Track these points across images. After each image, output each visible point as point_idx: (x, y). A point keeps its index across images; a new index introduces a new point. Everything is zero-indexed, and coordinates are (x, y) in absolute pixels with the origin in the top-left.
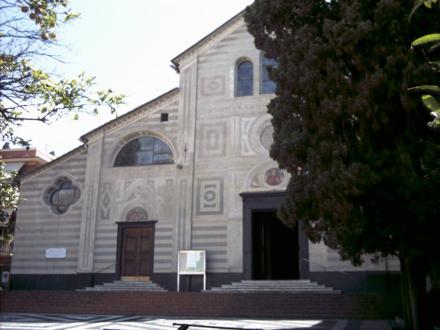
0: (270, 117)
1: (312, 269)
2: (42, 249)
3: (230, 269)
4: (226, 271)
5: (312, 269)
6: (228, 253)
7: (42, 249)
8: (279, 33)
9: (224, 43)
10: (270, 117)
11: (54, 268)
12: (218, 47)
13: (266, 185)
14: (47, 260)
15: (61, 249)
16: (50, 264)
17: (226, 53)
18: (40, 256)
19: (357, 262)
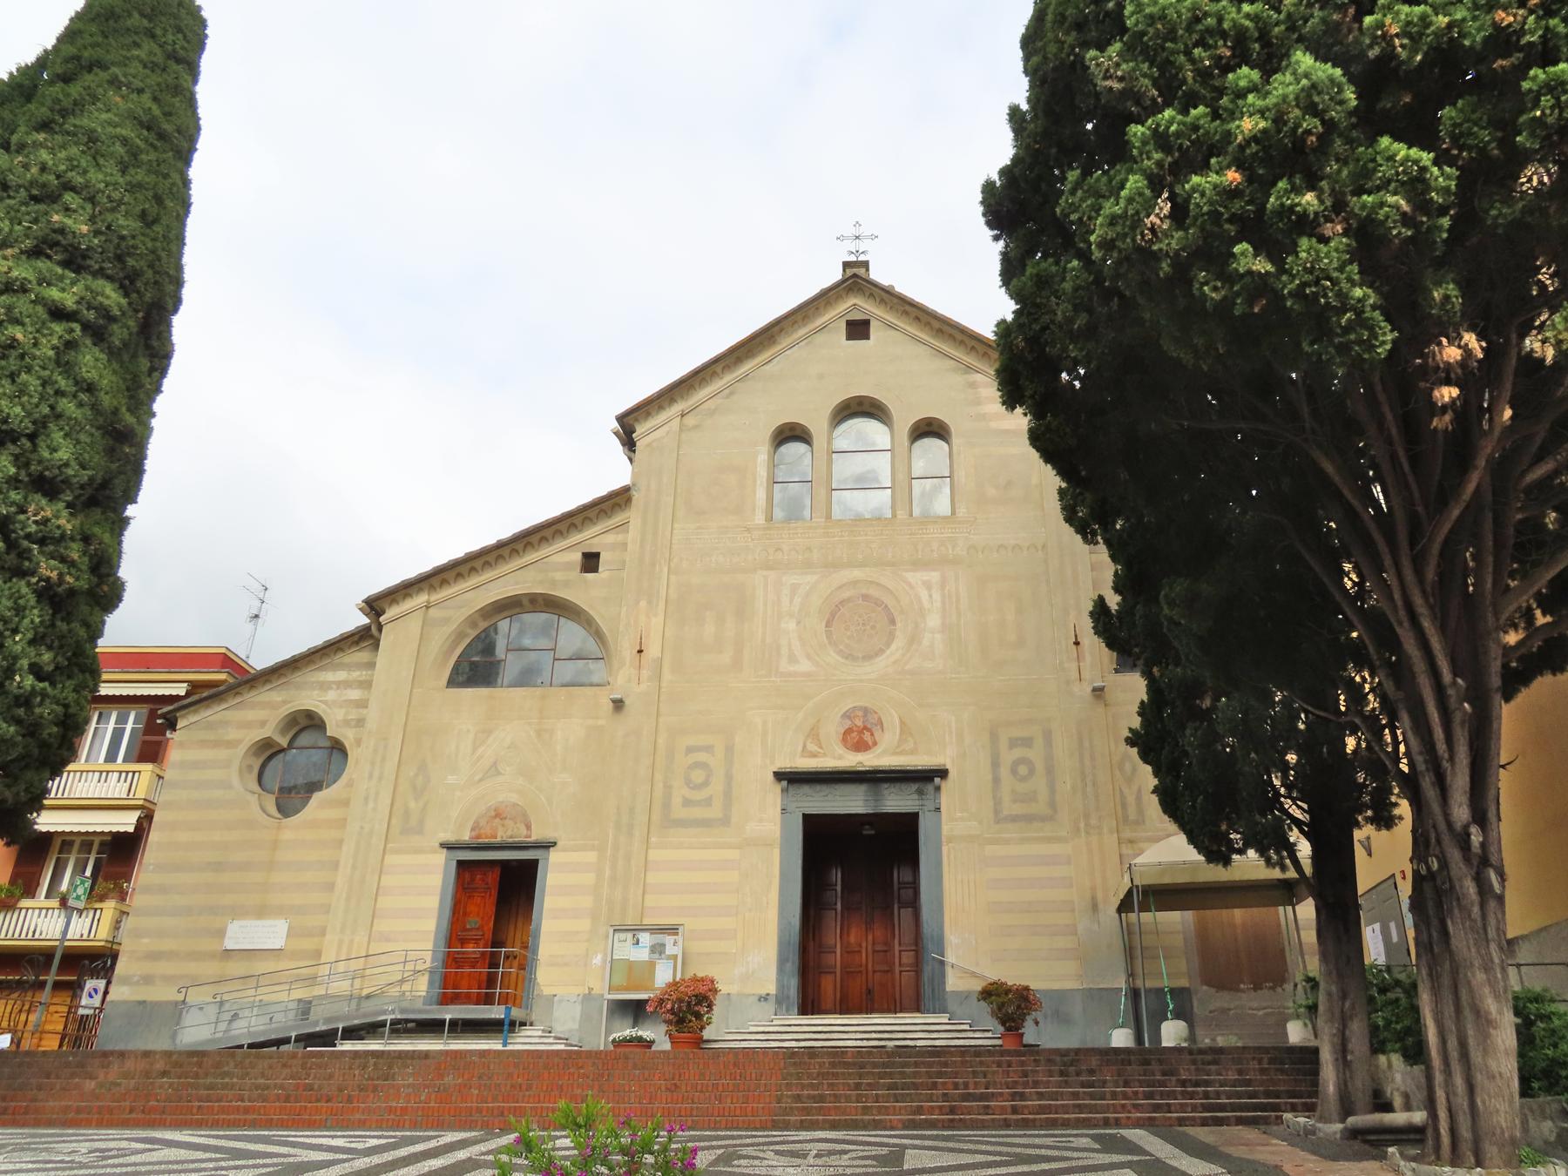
13: (840, 749)
14: (228, 953)
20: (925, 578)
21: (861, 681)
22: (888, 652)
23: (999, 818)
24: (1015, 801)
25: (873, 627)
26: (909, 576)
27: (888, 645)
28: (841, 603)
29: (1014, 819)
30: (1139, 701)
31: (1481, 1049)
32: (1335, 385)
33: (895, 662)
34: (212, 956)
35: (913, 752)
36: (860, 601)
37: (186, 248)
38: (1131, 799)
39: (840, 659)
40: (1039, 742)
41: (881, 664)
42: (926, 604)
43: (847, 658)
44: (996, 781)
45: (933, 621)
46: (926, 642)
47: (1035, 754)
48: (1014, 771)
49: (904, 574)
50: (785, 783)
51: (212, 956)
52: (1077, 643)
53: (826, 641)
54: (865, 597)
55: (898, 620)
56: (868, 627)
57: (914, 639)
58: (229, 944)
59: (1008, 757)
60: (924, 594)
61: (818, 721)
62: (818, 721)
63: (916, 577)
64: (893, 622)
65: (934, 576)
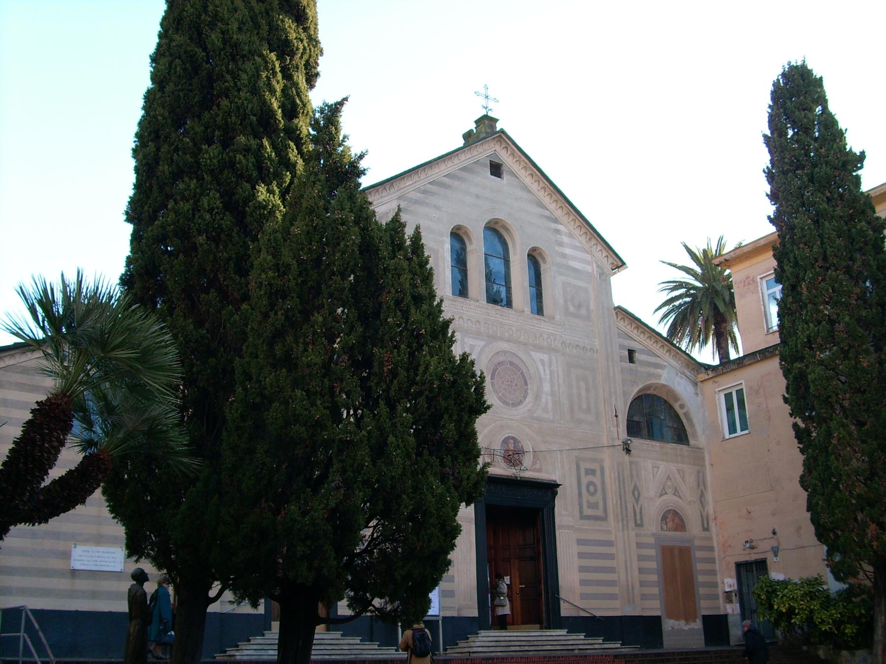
0: (30, 416)
1: (565, 611)
2: (61, 546)
3: (459, 609)
4: (455, 614)
5: (565, 611)
6: (456, 580)
7: (61, 546)
8: (436, 388)
9: (434, 188)
10: (30, 416)
11: (94, 595)
12: (425, 192)
13: (503, 465)
14: (74, 573)
15: (111, 550)
16: (81, 584)
17: (438, 208)
18: (55, 564)
19: (278, 108)
20: (541, 358)
21: (512, 420)
22: (525, 404)
23: (583, 517)
24: (589, 507)
25: (516, 385)
26: (533, 353)
27: (525, 397)
28: (499, 363)
29: (589, 518)
30: (825, 566)
31: (664, 522)
32: (371, 581)
33: (529, 410)
34: (60, 574)
35: (539, 470)
36: (508, 366)
37: (152, 48)
38: (638, 511)
39: (499, 402)
40: (598, 472)
41: (522, 410)
42: (543, 376)
43: (503, 403)
44: (580, 494)
45: (547, 387)
46: (543, 400)
47: (597, 480)
48: (588, 490)
49: (530, 352)
50: (823, 253)
51: (60, 574)
52: (616, 416)
53: (492, 389)
54: (511, 363)
55: (528, 382)
56: (514, 384)
57: (537, 397)
58: (77, 565)
59: (585, 480)
60: (541, 368)
61: (491, 443)
62: (491, 443)
63: (537, 356)
64: (526, 384)
65: (545, 357)
